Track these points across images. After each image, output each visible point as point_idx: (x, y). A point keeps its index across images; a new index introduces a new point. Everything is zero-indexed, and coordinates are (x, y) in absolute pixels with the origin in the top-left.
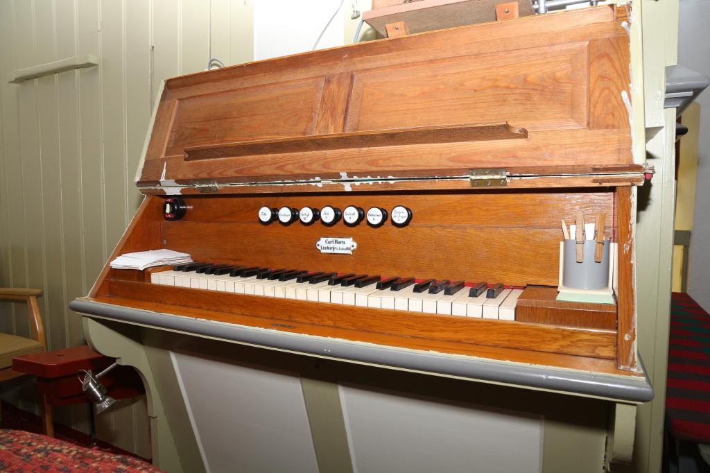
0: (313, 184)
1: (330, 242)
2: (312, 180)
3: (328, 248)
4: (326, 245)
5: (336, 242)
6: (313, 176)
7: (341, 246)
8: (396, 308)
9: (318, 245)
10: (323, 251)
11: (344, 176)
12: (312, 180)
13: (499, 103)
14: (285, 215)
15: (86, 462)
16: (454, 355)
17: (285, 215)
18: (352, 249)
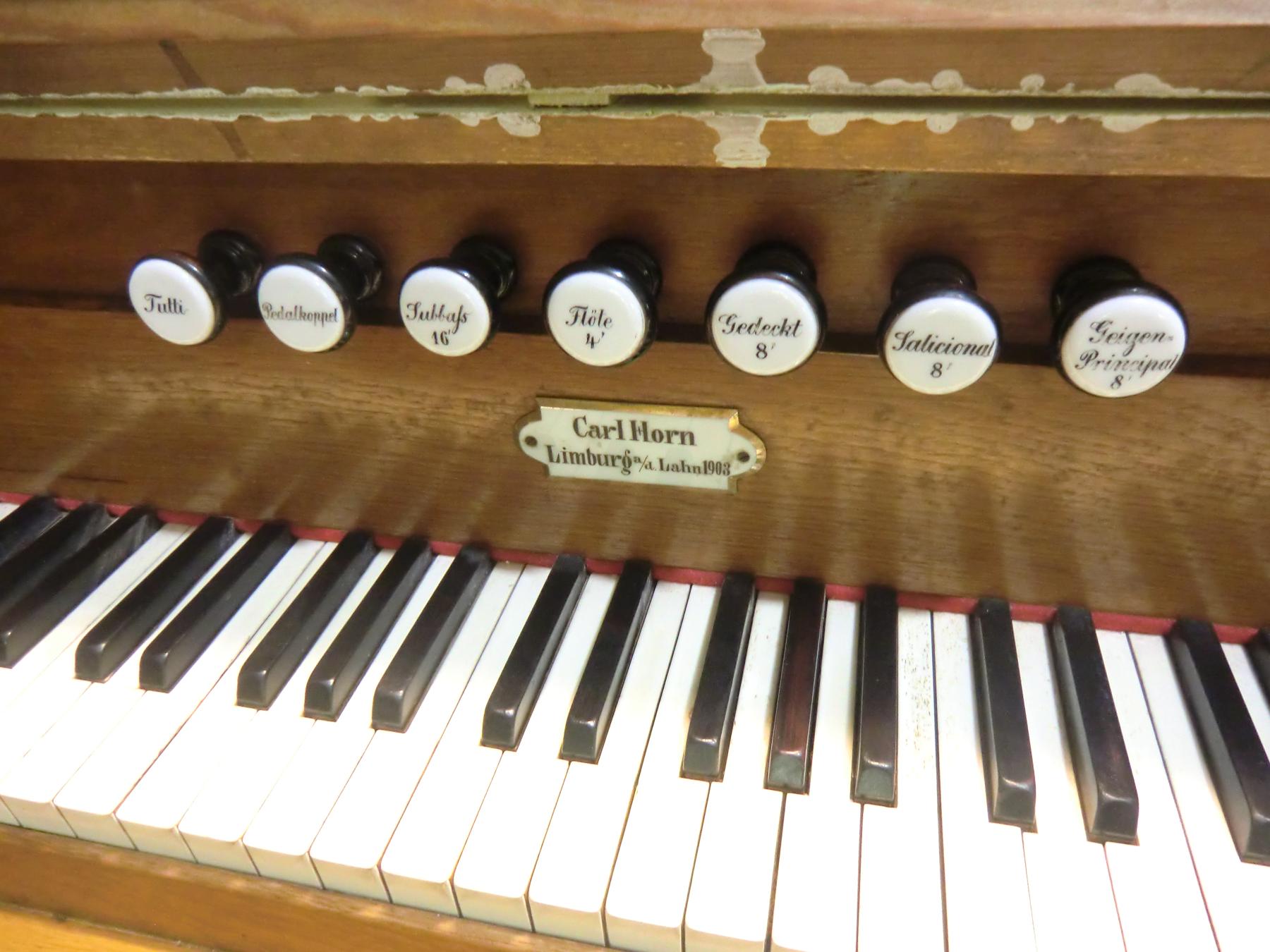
0: (472, 118)
1: (595, 431)
2: (456, 85)
3: (591, 458)
4: (580, 445)
5: (640, 431)
6: (474, 54)
7: (673, 452)
8: (707, 784)
9: (531, 441)
10: (557, 470)
11: (733, 56)
12: (456, 85)
13: (1227, 484)
14: (300, 314)
15: (306, 385)
16: (1210, 711)
17: (300, 314)
18: (739, 469)
